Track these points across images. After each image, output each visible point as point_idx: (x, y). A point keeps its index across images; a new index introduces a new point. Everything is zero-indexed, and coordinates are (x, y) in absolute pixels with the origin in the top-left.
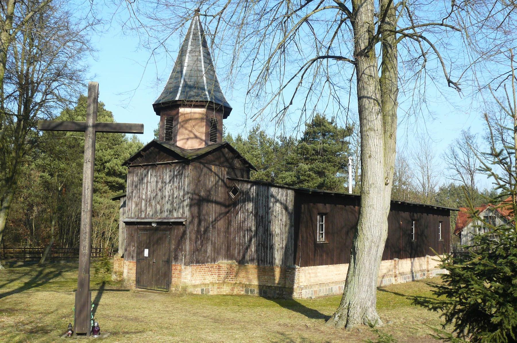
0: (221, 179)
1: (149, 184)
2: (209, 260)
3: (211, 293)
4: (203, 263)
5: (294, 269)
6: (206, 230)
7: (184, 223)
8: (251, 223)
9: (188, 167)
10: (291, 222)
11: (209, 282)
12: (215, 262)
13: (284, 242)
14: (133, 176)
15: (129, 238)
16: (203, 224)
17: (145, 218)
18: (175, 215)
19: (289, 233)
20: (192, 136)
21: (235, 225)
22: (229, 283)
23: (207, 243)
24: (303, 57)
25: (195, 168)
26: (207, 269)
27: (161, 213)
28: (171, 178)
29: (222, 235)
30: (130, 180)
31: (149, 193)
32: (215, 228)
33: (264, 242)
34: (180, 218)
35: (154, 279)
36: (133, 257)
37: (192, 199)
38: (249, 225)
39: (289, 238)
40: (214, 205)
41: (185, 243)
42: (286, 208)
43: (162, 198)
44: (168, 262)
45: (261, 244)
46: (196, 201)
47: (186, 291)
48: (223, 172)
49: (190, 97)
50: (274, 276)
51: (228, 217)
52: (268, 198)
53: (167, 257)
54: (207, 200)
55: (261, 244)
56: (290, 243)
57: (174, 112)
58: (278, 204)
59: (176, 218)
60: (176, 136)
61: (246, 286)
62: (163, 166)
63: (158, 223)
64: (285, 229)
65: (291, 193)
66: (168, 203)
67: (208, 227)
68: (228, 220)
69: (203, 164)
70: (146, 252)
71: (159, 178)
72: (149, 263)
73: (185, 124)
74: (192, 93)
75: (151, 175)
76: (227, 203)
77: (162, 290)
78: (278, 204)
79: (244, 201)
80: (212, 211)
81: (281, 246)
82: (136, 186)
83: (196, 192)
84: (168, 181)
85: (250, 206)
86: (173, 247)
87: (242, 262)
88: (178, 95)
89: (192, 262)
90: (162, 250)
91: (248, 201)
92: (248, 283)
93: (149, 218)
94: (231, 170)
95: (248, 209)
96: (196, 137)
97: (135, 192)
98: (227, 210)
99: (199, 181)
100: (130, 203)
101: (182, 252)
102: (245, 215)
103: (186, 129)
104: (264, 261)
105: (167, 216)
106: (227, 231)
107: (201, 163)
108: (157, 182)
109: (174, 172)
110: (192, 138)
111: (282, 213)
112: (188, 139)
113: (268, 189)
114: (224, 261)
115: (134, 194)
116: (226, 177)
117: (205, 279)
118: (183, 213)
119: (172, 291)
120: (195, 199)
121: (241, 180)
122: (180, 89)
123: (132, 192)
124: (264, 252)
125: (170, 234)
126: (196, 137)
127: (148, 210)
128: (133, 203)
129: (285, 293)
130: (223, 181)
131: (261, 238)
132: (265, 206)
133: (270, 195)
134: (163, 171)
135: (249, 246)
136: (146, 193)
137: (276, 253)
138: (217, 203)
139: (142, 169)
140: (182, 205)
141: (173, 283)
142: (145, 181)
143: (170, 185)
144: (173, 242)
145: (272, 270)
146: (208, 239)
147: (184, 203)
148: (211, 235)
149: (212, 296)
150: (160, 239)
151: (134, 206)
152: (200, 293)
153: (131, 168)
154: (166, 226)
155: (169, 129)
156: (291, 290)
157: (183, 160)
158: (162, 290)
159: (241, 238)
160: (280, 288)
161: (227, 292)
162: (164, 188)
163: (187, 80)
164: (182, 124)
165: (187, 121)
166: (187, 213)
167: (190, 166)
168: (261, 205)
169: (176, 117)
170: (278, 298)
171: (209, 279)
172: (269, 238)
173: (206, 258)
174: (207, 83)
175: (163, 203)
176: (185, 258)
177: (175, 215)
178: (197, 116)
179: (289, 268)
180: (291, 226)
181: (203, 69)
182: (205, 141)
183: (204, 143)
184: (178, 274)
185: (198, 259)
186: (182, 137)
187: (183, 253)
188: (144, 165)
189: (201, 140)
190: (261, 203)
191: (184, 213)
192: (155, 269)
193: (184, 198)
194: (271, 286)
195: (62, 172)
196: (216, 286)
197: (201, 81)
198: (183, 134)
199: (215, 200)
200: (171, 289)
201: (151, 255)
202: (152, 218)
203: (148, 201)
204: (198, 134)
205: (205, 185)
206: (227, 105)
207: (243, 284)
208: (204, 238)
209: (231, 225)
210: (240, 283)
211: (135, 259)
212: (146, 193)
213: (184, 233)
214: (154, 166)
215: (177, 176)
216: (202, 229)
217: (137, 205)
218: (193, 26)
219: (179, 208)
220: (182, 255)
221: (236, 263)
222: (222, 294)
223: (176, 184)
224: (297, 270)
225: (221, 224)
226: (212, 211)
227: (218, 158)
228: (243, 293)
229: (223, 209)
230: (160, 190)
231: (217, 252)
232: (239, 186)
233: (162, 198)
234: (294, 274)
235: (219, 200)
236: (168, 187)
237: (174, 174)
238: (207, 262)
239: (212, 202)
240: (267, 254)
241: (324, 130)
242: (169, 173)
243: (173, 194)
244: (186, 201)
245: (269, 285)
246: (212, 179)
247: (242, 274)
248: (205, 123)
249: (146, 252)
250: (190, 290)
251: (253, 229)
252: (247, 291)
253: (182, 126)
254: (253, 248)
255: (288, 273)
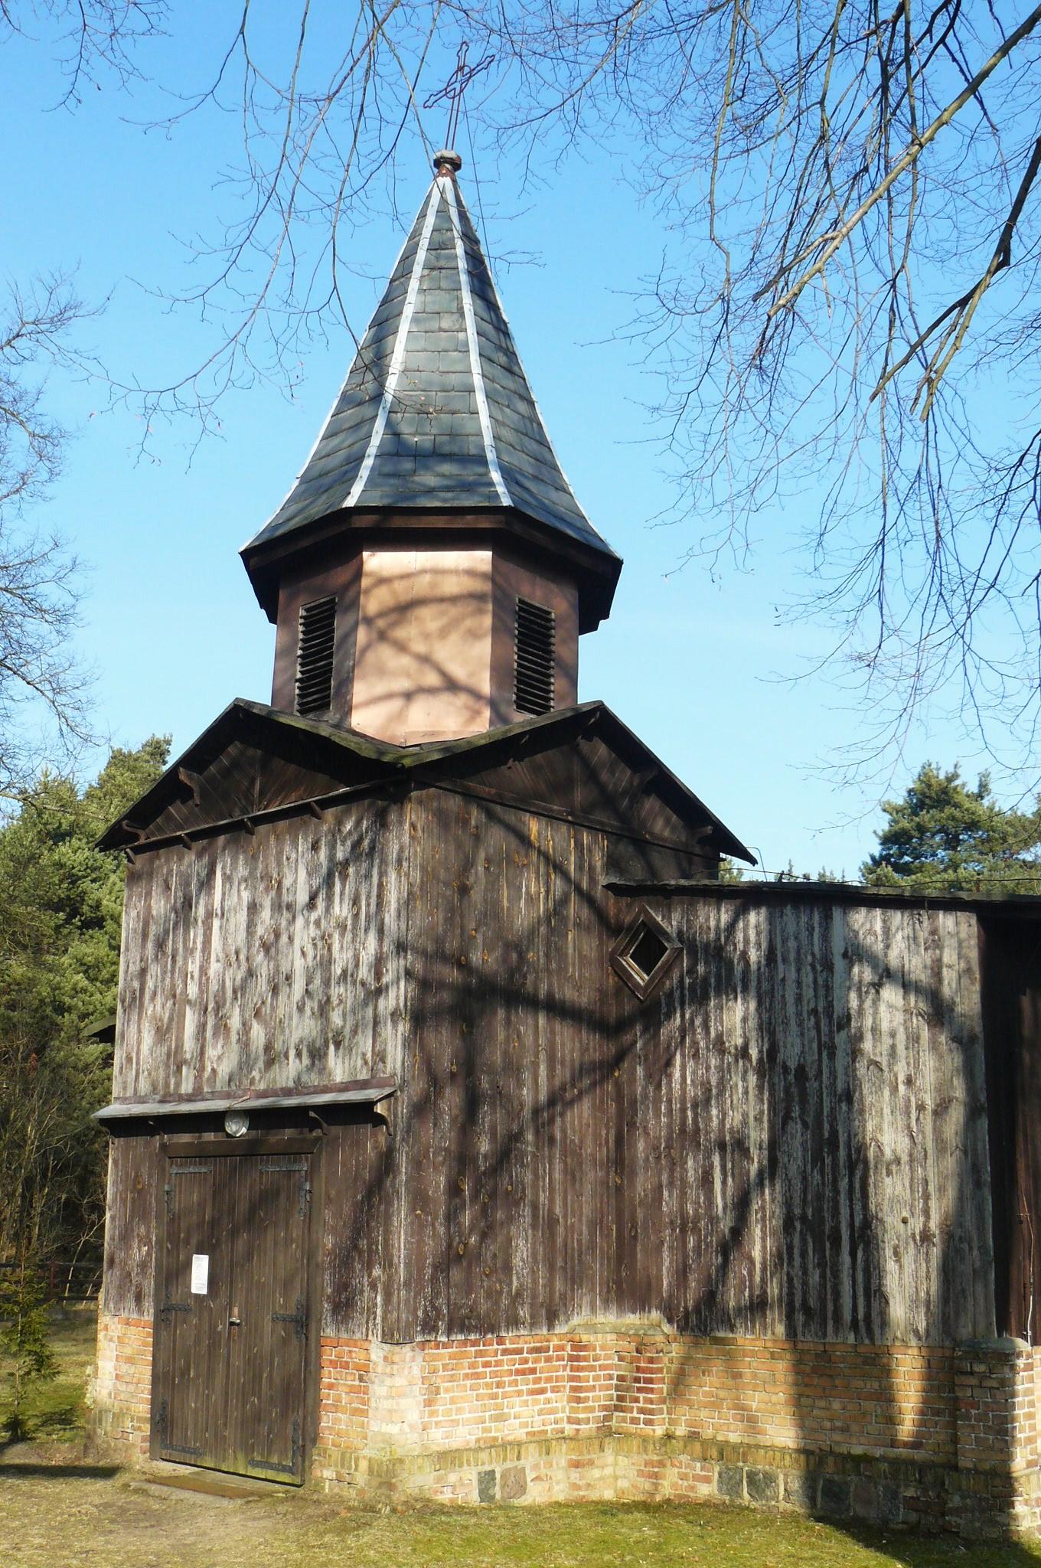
0: (578, 889)
1: (216, 923)
2: (524, 1312)
3: (535, 1495)
4: (486, 1326)
5: (1007, 1358)
6: (506, 1153)
7: (379, 1109)
8: (744, 1107)
9: (401, 815)
10: (971, 1090)
11: (520, 1434)
12: (552, 1318)
13: (933, 1204)
14: (149, 894)
15: (124, 1201)
16: (487, 1116)
17: (196, 1095)
18: (338, 1068)
19: (968, 1149)
20: (432, 679)
21: (656, 1124)
22: (628, 1435)
23: (510, 1220)
24: (1009, 166)
25: (442, 819)
26: (509, 1363)
27: (270, 1063)
28: (316, 882)
29: (591, 1176)
30: (133, 914)
31: (214, 968)
32: (552, 1140)
33: (819, 1210)
34: (364, 1085)
35: (235, 1414)
36: (139, 1298)
37: (425, 986)
38: (734, 1119)
39: (970, 1173)
40: (542, 1021)
41: (388, 1218)
42: (939, 1012)
43: (275, 990)
44: (302, 1325)
45: (803, 1218)
46: (446, 997)
47: (391, 1487)
48: (585, 854)
49: (415, 495)
50: (886, 1396)
51: (618, 1085)
52: (829, 967)
53: (297, 1295)
54: (508, 992)
55: (803, 1218)
56: (969, 1207)
57: (340, 576)
58: (891, 994)
59: (345, 1087)
60: (347, 682)
61: (724, 1451)
62: (282, 824)
63: (254, 1116)
64: (937, 1131)
65: (958, 932)
66: (301, 1009)
67: (516, 1137)
68: (619, 1098)
69: (483, 802)
70: (200, 1268)
71: (261, 887)
72: (213, 1328)
73: (394, 625)
74: (429, 479)
75: (228, 879)
76: (613, 1013)
77: (270, 1474)
78: (891, 994)
79: (699, 995)
80: (537, 1054)
81: (917, 1225)
82: (160, 945)
83: (452, 945)
84: (302, 897)
85: (736, 1017)
86: (329, 1241)
87: (704, 1320)
88: (357, 489)
89: (429, 1327)
90: (275, 1259)
91: (718, 994)
92: (734, 1438)
93: (214, 1095)
94: (625, 849)
95: (720, 1038)
96: (452, 685)
97: (154, 970)
98: (610, 1049)
99: (464, 890)
100: (133, 1028)
101: (369, 1267)
102: (716, 1067)
103: (401, 647)
104: (828, 1310)
105: (298, 1081)
106: (620, 1161)
107: (469, 796)
108: (253, 908)
109: (332, 847)
110: (431, 691)
111: (914, 1039)
112: (408, 696)
113: (827, 918)
114: (601, 1318)
115: (150, 984)
116: (603, 880)
117: (500, 1418)
118: (376, 1057)
119: (318, 1488)
120: (441, 985)
121: (680, 891)
122: (368, 463)
123: (143, 972)
124: (822, 1265)
125: (310, 1175)
126: (452, 685)
127: (212, 1053)
128: (146, 1025)
129: (956, 1501)
130: (588, 898)
131: (798, 1185)
132: (814, 1012)
133: (838, 947)
134: (280, 853)
135: (738, 1232)
136: (203, 971)
137: (891, 1265)
138: (556, 1009)
139: (190, 857)
140: (370, 1011)
141: (328, 1438)
142: (201, 912)
143: (314, 916)
144: (328, 1215)
145: (876, 1366)
146: (514, 1200)
147: (381, 1002)
148: (528, 1178)
149: (534, 1511)
150: (267, 1199)
151: (148, 1039)
152: (474, 1498)
153: (140, 860)
154: (295, 1128)
155: (319, 671)
156: (999, 1488)
157: (381, 780)
158: (270, 1474)
159: (692, 1193)
160: (923, 1468)
161: (622, 1484)
162: (284, 939)
163: (405, 429)
164: (381, 623)
165: (404, 609)
166: (396, 1056)
167: (409, 807)
168: (791, 1009)
169: (351, 593)
170: (913, 1530)
171: (526, 1413)
172: (843, 1184)
173: (505, 1301)
174: (496, 438)
175: (280, 1012)
176: (387, 1300)
177: (338, 1068)
178: (452, 586)
179: (976, 1351)
180: (973, 1113)
181: (478, 381)
182: (493, 704)
183: (487, 713)
184: (352, 1390)
185: (461, 1306)
186: (381, 687)
187: (377, 1272)
188: (195, 836)
189: (476, 695)
190: (790, 999)
191: (380, 1056)
192: (237, 1362)
193: (378, 975)
194: (866, 1459)
195: (19, 991)
196: (562, 1456)
197: (469, 428)
198: (381, 671)
199: (550, 995)
200: (317, 1472)
201: (223, 1289)
202: (228, 1096)
203: (213, 1010)
204: (459, 672)
205: (493, 913)
206: (598, 545)
207: (705, 1443)
208: (492, 1196)
209: (632, 1125)
210: (693, 1436)
211: (149, 1305)
212: (203, 971)
213: (386, 1163)
214: (240, 830)
215: (346, 864)
216: (484, 1146)
217: (161, 1033)
218: (430, 220)
219: (355, 1032)
220: (373, 1286)
221: (667, 1328)
222: (594, 1496)
223: (341, 910)
224: (1021, 1363)
225: (582, 1121)
226: (537, 1054)
227: (561, 788)
228: (706, 1490)
229: (596, 1047)
230: (266, 947)
231: (994, 1523)
232: (671, 922)
233: (275, 990)
234: (1004, 1392)
235: (568, 994)
236: (303, 932)
237: (331, 858)
238: (514, 1322)
239: (533, 1003)
240: (836, 1274)
241: (953, 818)
242: (308, 856)
243: (326, 963)
244: (392, 993)
245: (857, 1450)
246: (531, 883)
247: (708, 1385)
248: (487, 621)
249: (200, 1268)
250: (419, 1481)
251: (758, 1135)
252: (730, 1482)
253: (382, 636)
254: (759, 1244)
255: (971, 1379)
